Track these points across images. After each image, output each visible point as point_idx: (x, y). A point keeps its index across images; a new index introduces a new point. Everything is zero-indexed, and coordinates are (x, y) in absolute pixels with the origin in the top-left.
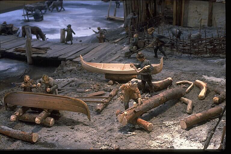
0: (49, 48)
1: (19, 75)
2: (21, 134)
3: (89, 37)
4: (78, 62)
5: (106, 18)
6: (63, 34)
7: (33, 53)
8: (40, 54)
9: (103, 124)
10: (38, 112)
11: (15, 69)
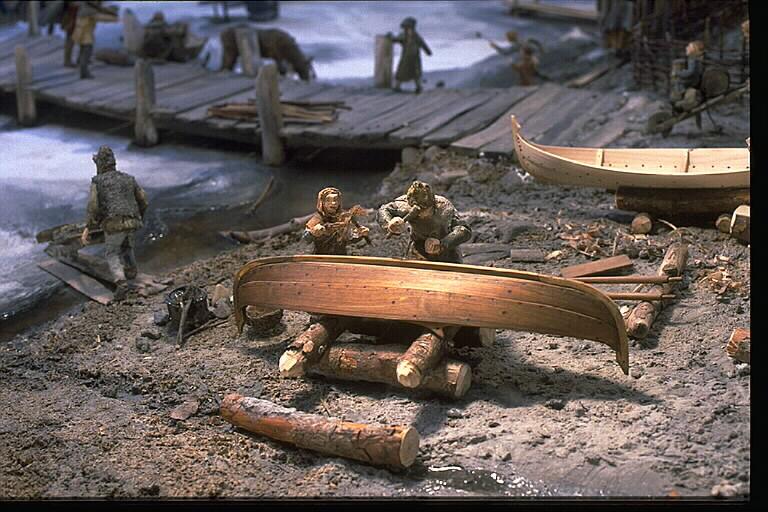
0: (343, 103)
1: (242, 203)
2: (344, 433)
3: (466, 70)
4: (474, 153)
5: (507, 8)
6: (385, 55)
7: (286, 124)
8: (311, 124)
9: (677, 387)
10: (373, 339)
11: (219, 183)
